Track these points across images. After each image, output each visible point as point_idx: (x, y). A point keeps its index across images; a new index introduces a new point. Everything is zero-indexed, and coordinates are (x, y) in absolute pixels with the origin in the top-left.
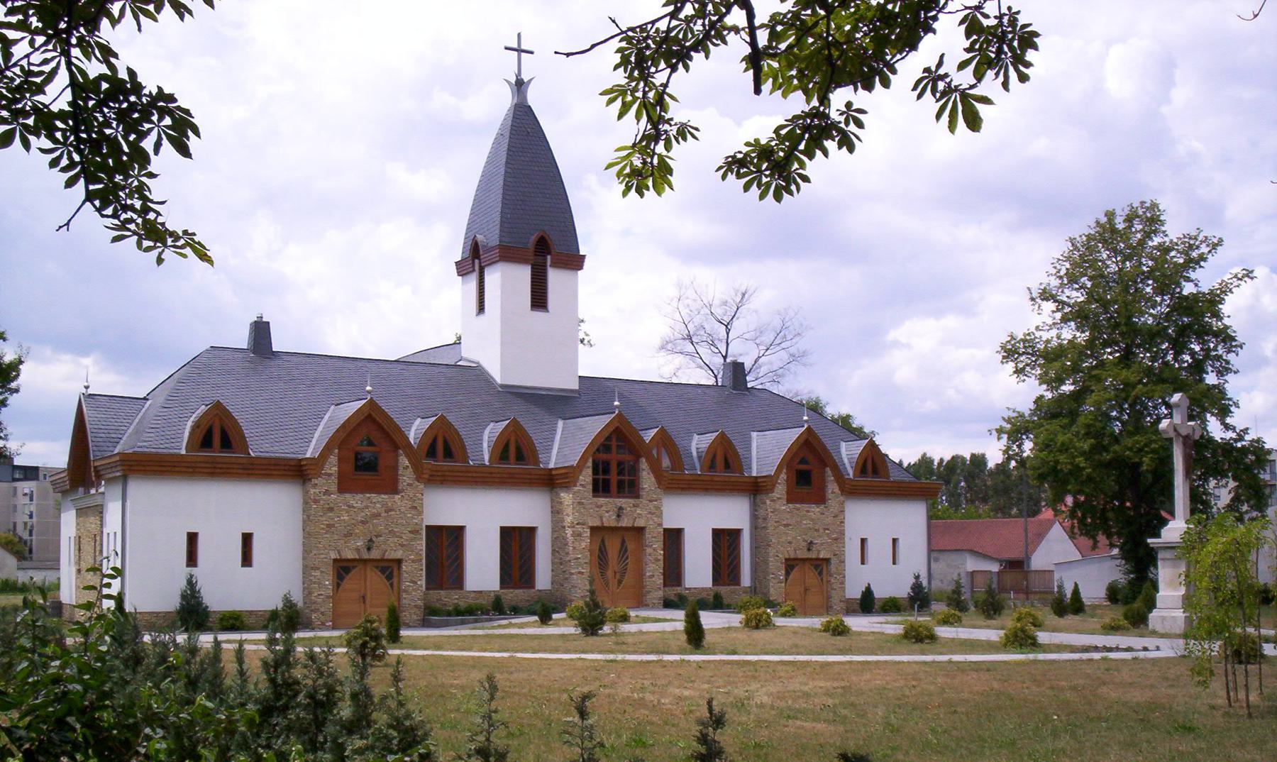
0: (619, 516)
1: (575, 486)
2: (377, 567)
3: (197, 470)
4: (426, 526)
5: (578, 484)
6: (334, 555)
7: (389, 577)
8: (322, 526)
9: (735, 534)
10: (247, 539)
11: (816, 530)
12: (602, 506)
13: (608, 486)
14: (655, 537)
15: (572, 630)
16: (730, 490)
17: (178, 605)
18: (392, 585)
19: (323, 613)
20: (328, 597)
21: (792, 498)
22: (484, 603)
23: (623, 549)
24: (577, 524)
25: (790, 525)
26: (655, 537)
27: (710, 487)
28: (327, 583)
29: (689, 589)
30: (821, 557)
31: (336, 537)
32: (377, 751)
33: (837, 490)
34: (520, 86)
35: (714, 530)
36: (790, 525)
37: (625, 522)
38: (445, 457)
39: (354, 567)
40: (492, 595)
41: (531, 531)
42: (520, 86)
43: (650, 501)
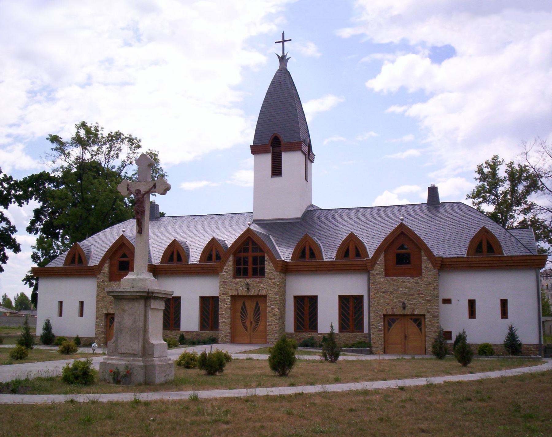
0: (248, 289)
1: (222, 272)
2: (411, 319)
3: (60, 273)
4: (296, 298)
5: (223, 271)
6: (105, 312)
7: (419, 325)
8: (100, 297)
9: (359, 299)
10: (504, 303)
11: (411, 295)
12: (238, 283)
13: (253, 271)
14: (273, 301)
15: (317, 357)
16: (348, 270)
17: (519, 339)
18: (421, 330)
19: (100, 340)
20: (102, 332)
21: (388, 273)
22: (189, 338)
23: (257, 309)
24: (223, 294)
25: (388, 292)
26: (273, 301)
27: (331, 269)
28: (101, 325)
29: (321, 334)
30: (416, 313)
31: (106, 303)
32: (107, 410)
33: (430, 266)
34: (283, 59)
35: (341, 297)
36: (388, 292)
37: (253, 292)
38: (310, 257)
39: (397, 319)
40: (194, 333)
41: (360, 298)
42: (283, 59)
43: (270, 279)
